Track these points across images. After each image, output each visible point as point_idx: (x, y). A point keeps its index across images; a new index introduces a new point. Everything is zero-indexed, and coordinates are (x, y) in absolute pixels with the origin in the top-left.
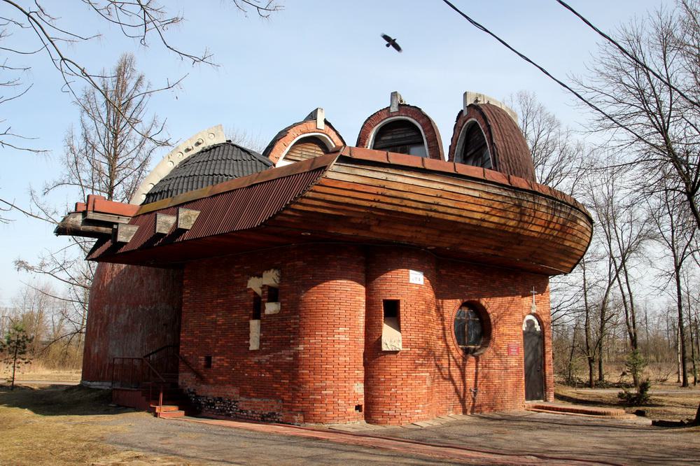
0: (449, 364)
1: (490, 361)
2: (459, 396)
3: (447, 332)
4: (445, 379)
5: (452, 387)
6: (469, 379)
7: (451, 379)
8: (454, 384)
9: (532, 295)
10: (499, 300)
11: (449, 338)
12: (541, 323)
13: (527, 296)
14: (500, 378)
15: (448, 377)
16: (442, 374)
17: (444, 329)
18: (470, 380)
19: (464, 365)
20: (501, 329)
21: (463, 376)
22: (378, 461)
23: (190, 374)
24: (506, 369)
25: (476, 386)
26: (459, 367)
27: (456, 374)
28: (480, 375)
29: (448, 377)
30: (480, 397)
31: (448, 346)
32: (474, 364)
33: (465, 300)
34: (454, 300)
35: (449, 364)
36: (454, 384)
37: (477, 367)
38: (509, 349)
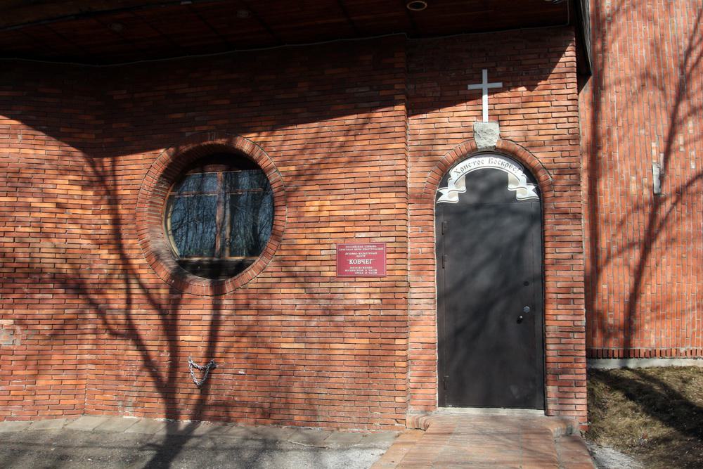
0: (129, 301)
1: (267, 291)
2: (156, 376)
3: (124, 230)
4: (114, 334)
5: (134, 354)
6: (188, 338)
7: (132, 334)
8: (139, 343)
9: (478, 95)
10: (303, 132)
11: (41, 287)
12: (532, 175)
13: (453, 103)
14: (301, 336)
15: (122, 330)
16: (105, 323)
17: (116, 222)
18: (193, 338)
19: (176, 304)
20: (312, 207)
21: (170, 329)
22: (28, 154)
23: (650, 374)
24: (329, 312)
25: (210, 353)
26: (156, 305)
27: (148, 323)
28: (226, 329)
29: (122, 330)
30: (230, 380)
31: (125, 260)
32: (207, 301)
33: (184, 149)
34: (148, 154)
35: (129, 301)
36: (139, 343)
37: (217, 307)
38: (341, 260)
